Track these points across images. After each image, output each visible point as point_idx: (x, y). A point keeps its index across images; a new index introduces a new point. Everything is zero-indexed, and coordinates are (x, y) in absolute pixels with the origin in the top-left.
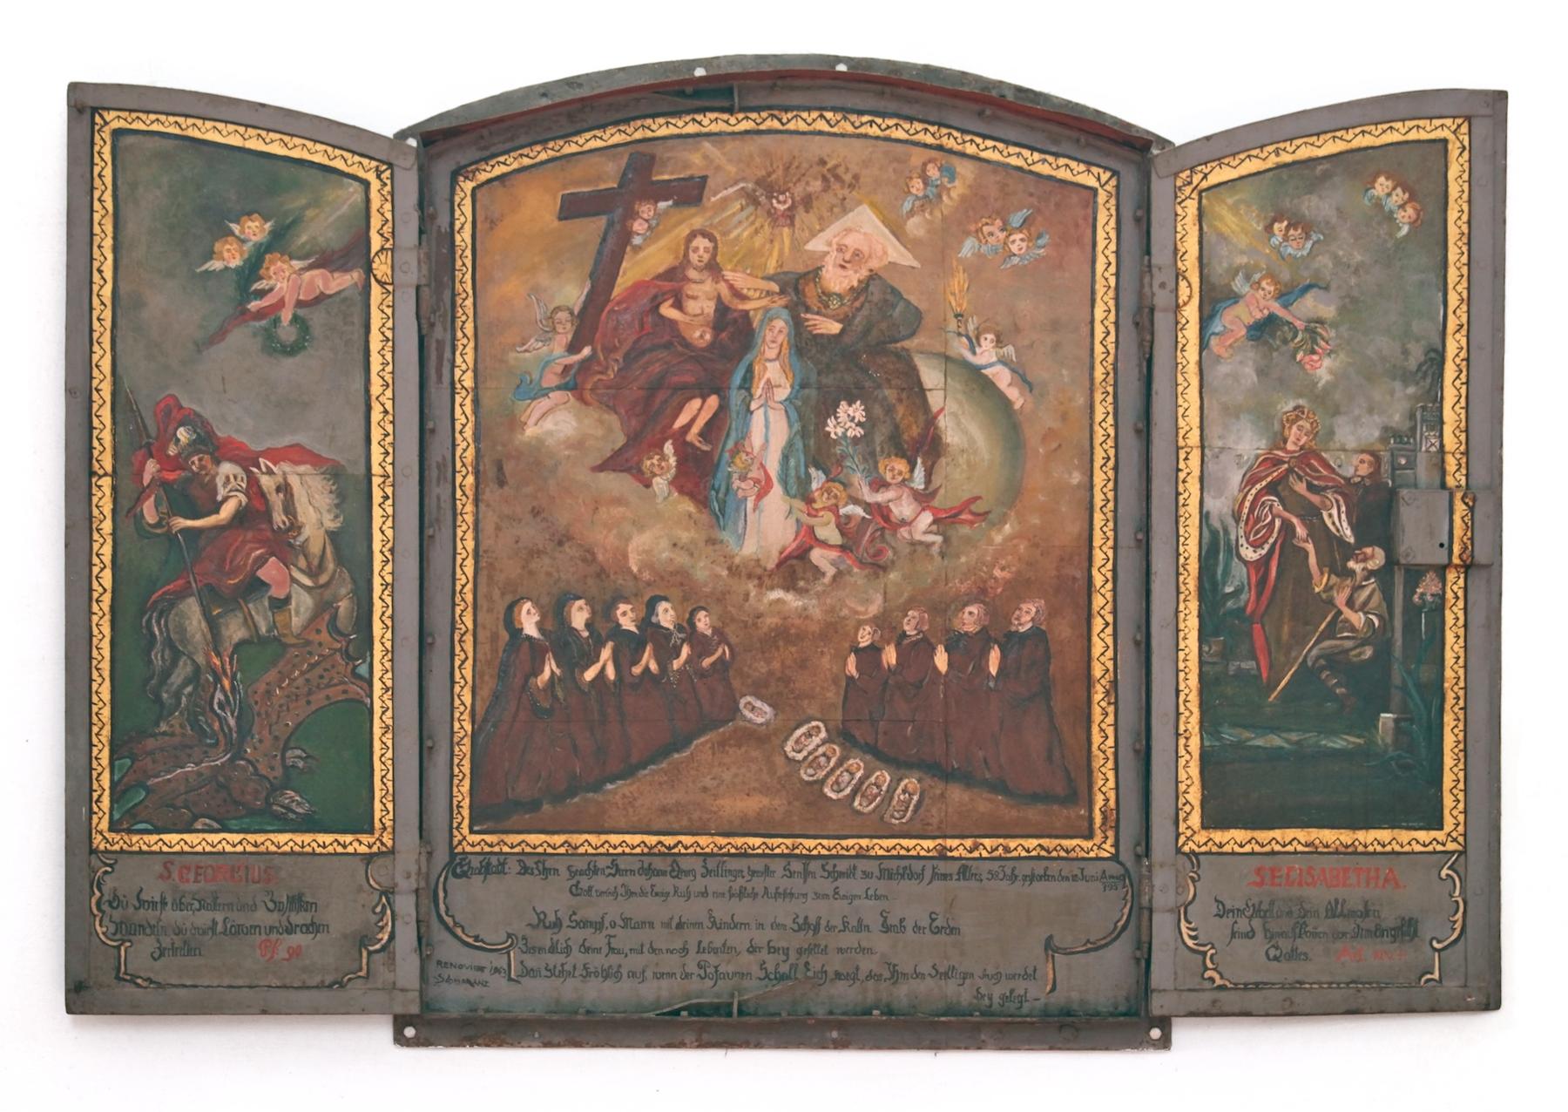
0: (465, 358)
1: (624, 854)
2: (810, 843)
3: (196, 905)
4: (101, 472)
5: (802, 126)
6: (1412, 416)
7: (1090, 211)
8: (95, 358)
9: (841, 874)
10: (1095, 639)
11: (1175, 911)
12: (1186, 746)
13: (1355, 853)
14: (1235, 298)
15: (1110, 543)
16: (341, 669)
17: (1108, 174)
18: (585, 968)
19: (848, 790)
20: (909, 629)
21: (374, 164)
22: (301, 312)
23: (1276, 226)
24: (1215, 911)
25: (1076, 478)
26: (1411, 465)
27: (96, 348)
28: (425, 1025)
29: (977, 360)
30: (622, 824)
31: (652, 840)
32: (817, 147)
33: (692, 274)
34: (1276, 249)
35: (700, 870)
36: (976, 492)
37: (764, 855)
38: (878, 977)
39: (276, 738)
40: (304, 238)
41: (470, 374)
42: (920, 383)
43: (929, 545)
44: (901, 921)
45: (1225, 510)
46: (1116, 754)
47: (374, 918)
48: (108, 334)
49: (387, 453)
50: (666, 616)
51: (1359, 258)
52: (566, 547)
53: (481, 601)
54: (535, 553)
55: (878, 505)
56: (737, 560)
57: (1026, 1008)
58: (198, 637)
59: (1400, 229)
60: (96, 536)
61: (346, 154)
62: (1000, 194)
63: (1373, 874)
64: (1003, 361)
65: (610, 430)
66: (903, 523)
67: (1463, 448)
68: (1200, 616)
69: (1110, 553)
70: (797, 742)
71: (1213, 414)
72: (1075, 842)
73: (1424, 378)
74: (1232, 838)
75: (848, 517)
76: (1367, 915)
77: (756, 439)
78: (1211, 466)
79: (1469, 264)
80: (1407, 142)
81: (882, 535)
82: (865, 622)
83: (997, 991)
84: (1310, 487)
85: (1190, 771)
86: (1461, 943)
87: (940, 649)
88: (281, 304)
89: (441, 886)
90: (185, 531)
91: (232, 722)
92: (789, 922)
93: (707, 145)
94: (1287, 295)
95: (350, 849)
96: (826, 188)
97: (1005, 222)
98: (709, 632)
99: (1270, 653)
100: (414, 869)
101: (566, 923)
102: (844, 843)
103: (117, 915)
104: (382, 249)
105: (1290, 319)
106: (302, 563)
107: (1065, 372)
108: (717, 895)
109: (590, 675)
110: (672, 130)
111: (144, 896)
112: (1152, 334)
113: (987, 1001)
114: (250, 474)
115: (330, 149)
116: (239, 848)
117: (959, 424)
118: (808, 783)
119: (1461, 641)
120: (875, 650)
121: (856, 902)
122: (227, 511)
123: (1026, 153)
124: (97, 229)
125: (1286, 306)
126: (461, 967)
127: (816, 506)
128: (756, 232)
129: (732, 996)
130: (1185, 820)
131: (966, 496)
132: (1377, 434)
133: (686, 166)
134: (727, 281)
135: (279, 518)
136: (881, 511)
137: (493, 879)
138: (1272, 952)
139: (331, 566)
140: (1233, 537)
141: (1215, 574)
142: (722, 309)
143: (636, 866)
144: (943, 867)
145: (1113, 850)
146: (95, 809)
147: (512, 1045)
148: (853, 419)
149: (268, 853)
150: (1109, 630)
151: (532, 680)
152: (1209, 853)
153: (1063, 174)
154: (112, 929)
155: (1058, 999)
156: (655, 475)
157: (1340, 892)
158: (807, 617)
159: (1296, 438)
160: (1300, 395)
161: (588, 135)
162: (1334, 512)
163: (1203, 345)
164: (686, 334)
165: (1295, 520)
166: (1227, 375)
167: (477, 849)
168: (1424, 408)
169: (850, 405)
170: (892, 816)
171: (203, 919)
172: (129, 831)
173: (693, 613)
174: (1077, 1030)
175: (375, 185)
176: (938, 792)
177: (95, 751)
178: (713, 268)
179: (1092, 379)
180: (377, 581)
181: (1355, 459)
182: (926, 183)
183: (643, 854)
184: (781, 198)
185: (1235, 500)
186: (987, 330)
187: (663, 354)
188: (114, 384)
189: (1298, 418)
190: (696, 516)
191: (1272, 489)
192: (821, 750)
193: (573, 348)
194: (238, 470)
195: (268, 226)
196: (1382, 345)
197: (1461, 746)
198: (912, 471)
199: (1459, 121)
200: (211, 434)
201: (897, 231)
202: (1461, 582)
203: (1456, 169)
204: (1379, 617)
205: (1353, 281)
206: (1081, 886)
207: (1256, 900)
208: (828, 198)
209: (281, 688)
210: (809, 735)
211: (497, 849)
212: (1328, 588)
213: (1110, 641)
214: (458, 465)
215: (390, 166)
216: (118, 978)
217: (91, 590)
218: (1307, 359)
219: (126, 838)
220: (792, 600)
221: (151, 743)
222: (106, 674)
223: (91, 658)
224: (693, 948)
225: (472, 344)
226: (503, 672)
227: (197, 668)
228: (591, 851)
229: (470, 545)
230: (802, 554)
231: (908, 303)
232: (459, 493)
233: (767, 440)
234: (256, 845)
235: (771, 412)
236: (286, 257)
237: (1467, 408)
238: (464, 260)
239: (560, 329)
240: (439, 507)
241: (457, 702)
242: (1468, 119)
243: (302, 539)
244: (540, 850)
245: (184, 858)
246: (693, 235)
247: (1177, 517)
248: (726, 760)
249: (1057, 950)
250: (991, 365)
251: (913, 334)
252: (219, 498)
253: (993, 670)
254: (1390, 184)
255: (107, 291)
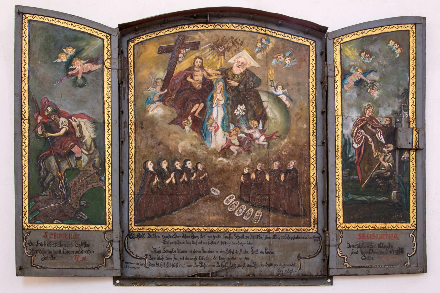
0: (131, 92)
1: (178, 232)
2: (231, 229)
3: (55, 245)
4: (25, 119)
5: (227, 28)
6: (400, 108)
7: (308, 52)
8: (23, 85)
9: (240, 237)
10: (311, 171)
11: (336, 246)
12: (338, 200)
13: (386, 230)
14: (351, 74)
15: (315, 144)
16: (96, 178)
17: (313, 42)
18: (167, 264)
19: (242, 214)
20: (259, 169)
21: (105, 34)
22: (84, 75)
23: (362, 54)
24: (347, 246)
25: (305, 126)
26: (400, 121)
27: (23, 83)
28: (122, 279)
29: (277, 93)
30: (177, 223)
31: (186, 228)
32: (231, 34)
33: (196, 69)
34: (362, 60)
35: (200, 236)
36: (277, 130)
37: (218, 232)
38: (251, 266)
39: (78, 197)
40: (85, 54)
41: (133, 97)
42: (261, 99)
43: (264, 145)
44: (257, 250)
45: (349, 133)
46: (317, 203)
47: (107, 249)
48: (27, 79)
49: (109, 117)
50: (189, 165)
51: (385, 63)
52: (161, 146)
53: (137, 161)
54: (153, 147)
55: (250, 134)
56: (209, 149)
57: (292, 274)
58: (54, 167)
59: (396, 55)
60: (23, 137)
61: (97, 31)
62: (283, 47)
63: (391, 235)
64: (284, 94)
65: (173, 112)
66: (257, 139)
67: (414, 117)
68: (342, 163)
69: (315, 147)
70: (227, 200)
71: (345, 106)
72: (306, 228)
73: (404, 97)
74: (352, 226)
75: (241, 137)
76: (390, 247)
77: (215, 115)
78: (345, 121)
79: (416, 65)
80: (398, 31)
81: (250, 142)
82: (246, 167)
83: (284, 270)
84: (373, 127)
85: (340, 207)
86: (416, 255)
87: (267, 174)
88: (78, 73)
89: (126, 241)
90: (51, 137)
91: (65, 192)
92: (225, 251)
93: (200, 33)
94: (365, 73)
95: (100, 229)
96: (234, 45)
97: (284, 55)
98: (202, 169)
99: (362, 174)
100: (119, 235)
101: (162, 251)
102: (241, 228)
103: (31, 247)
104: (108, 59)
105: (366, 80)
106: (85, 147)
107: (301, 97)
108: (205, 243)
109: (168, 181)
110: (190, 29)
111: (39, 242)
112: (328, 84)
113: (281, 272)
114: (69, 121)
115: (92, 29)
116: (67, 229)
117: (272, 111)
118: (231, 212)
119: (415, 171)
120: (249, 174)
121: (244, 245)
122: (63, 131)
123: (290, 36)
124: (23, 48)
125: (365, 76)
126: (132, 263)
127: (232, 134)
128: (214, 57)
129: (210, 271)
130: (338, 221)
131: (274, 131)
132: (391, 112)
133: (194, 39)
134: (206, 71)
135: (78, 134)
136: (250, 135)
137: (141, 239)
138: (363, 258)
139: (93, 148)
140: (351, 141)
141: (346, 152)
142: (204, 79)
143: (181, 235)
144: (268, 235)
145: (316, 230)
146: (24, 217)
147: (147, 286)
148: (242, 110)
149: (76, 230)
150: (315, 169)
151: (151, 183)
152: (345, 230)
153: (300, 42)
154: (30, 251)
155: (301, 272)
156: (186, 125)
157: (382, 241)
158: (229, 165)
159: (368, 113)
160: (369, 102)
161: (166, 30)
162: (379, 134)
163: (342, 87)
164: (194, 86)
165: (368, 137)
166: (349, 96)
167: (136, 230)
168: (404, 106)
169: (241, 106)
170: (254, 221)
171: (57, 249)
172: (34, 223)
173: (197, 164)
174: (307, 280)
175: (106, 40)
176: (267, 214)
177: (24, 200)
178: (202, 67)
179: (309, 99)
180: (107, 153)
181: (385, 120)
182: (262, 44)
183: (183, 232)
184: (221, 48)
185: (351, 131)
186: (280, 85)
187: (188, 91)
188: (29, 93)
189: (369, 108)
190: (197, 137)
191: (362, 127)
192: (234, 203)
193: (162, 90)
194: (66, 120)
195: (74, 50)
196: (392, 88)
197: (415, 200)
198: (259, 124)
199: (413, 25)
200: (58, 109)
201: (254, 57)
202: (414, 154)
203: (412, 39)
204: (392, 164)
205: (384, 70)
206: (307, 240)
207: (358, 243)
208: (234, 48)
209: (79, 183)
210: (230, 198)
211: (142, 230)
212: (378, 156)
213: (315, 172)
214: (130, 122)
215: (110, 35)
216: (31, 266)
217: (22, 153)
218: (371, 91)
219: (33, 225)
220: (225, 161)
221: (41, 198)
222: (27, 177)
223: (22, 173)
224: (198, 259)
225: (133, 89)
226: (144, 181)
227: (54, 177)
228: (169, 231)
229: (133, 145)
230: (228, 147)
231: (257, 77)
232: (130, 130)
233: (218, 115)
234: (72, 228)
235: (218, 108)
236: (80, 60)
237: (416, 106)
238: (131, 65)
239: (158, 84)
240: (124, 135)
241: (130, 189)
242: (415, 24)
243: (84, 140)
244: (154, 231)
245: (51, 231)
246: (196, 58)
247: (335, 135)
248: (207, 206)
249: (301, 258)
250: (281, 95)
251: (258, 86)
252: (60, 128)
253: (282, 180)
254: (393, 42)
255: (27, 66)
